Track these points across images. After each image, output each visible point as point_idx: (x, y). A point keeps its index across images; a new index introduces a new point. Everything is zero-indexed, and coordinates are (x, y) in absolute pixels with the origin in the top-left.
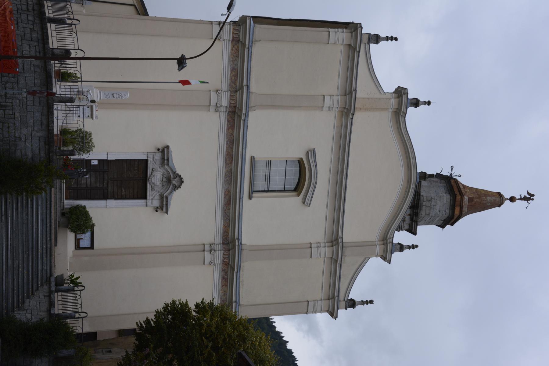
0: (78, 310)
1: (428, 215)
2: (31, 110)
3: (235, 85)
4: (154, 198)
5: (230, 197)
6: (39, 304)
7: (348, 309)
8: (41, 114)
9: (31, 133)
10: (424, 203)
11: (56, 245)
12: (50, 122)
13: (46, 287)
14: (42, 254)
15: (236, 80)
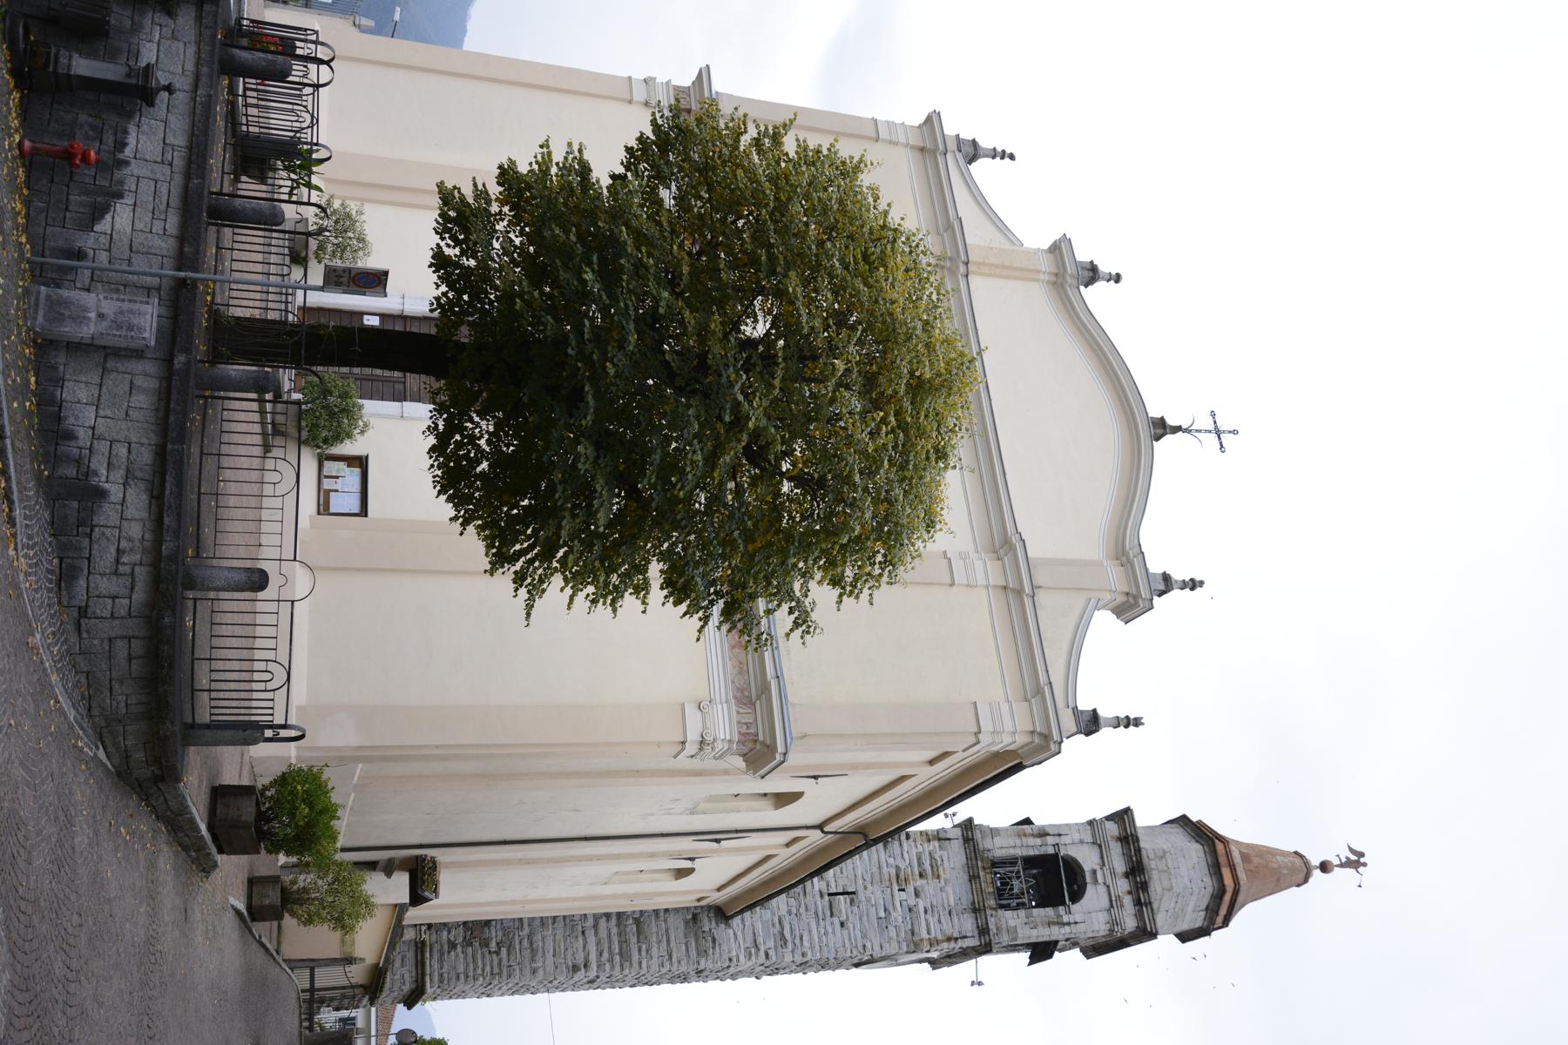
1: (1169, 890)
10: (1153, 864)
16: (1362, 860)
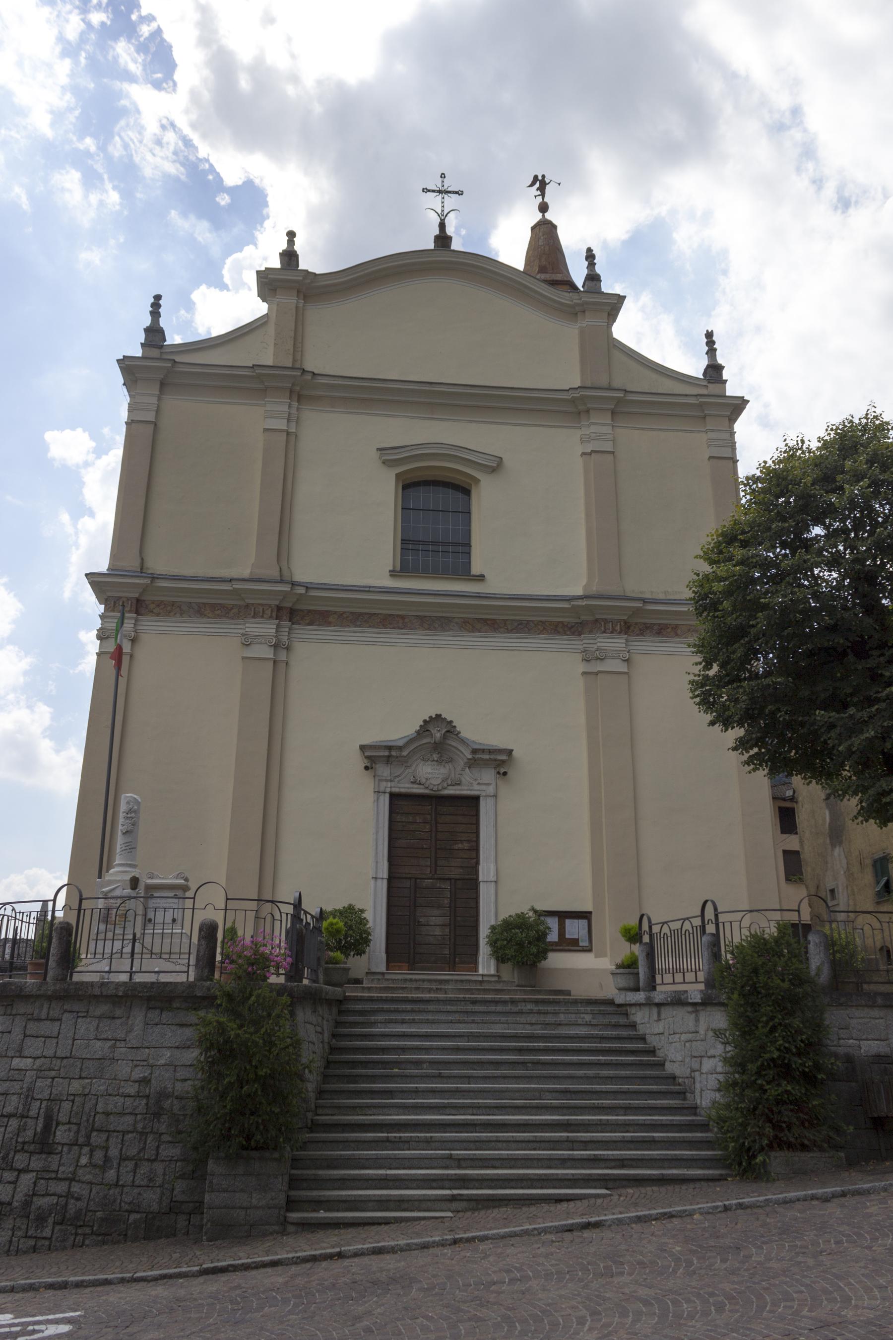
0: (696, 927)
2: (69, 1047)
3: (232, 609)
4: (476, 780)
5: (479, 620)
6: (678, 1036)
7: (724, 378)
8: (83, 1017)
9: (133, 1048)
11: (568, 993)
12: (105, 993)
13: (639, 1016)
14: (546, 1025)
15: (222, 606)
16: (540, 178)
